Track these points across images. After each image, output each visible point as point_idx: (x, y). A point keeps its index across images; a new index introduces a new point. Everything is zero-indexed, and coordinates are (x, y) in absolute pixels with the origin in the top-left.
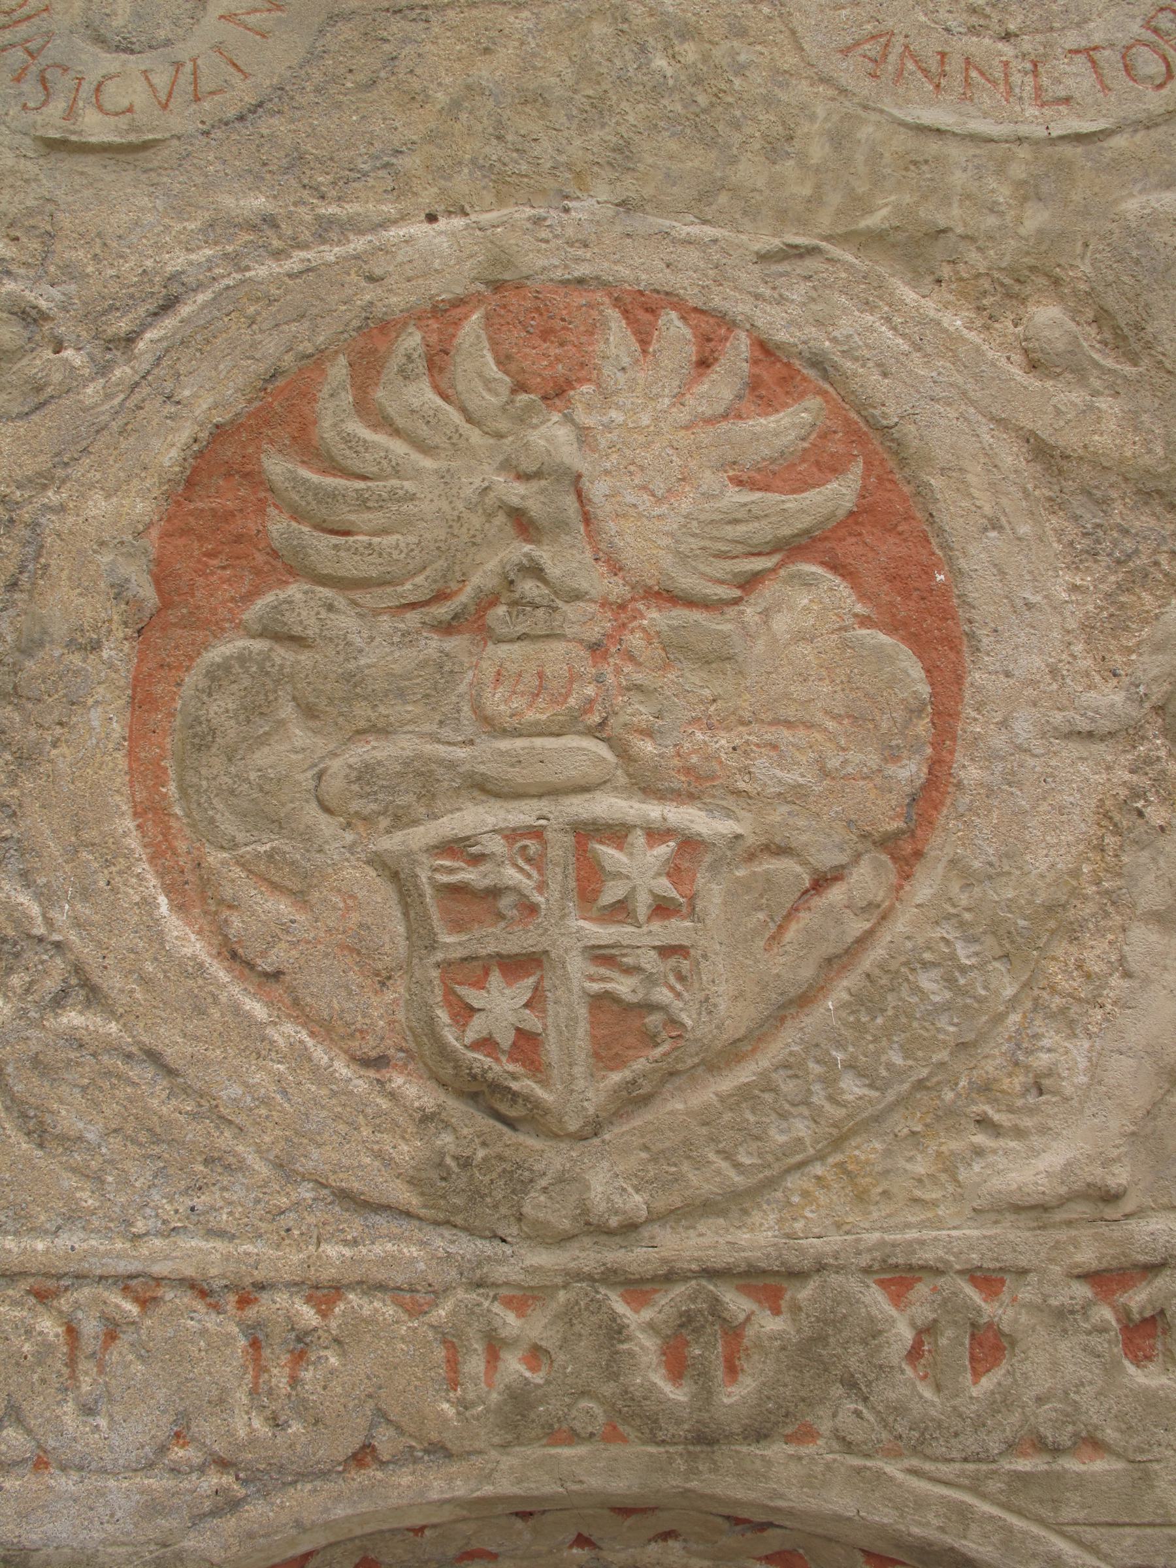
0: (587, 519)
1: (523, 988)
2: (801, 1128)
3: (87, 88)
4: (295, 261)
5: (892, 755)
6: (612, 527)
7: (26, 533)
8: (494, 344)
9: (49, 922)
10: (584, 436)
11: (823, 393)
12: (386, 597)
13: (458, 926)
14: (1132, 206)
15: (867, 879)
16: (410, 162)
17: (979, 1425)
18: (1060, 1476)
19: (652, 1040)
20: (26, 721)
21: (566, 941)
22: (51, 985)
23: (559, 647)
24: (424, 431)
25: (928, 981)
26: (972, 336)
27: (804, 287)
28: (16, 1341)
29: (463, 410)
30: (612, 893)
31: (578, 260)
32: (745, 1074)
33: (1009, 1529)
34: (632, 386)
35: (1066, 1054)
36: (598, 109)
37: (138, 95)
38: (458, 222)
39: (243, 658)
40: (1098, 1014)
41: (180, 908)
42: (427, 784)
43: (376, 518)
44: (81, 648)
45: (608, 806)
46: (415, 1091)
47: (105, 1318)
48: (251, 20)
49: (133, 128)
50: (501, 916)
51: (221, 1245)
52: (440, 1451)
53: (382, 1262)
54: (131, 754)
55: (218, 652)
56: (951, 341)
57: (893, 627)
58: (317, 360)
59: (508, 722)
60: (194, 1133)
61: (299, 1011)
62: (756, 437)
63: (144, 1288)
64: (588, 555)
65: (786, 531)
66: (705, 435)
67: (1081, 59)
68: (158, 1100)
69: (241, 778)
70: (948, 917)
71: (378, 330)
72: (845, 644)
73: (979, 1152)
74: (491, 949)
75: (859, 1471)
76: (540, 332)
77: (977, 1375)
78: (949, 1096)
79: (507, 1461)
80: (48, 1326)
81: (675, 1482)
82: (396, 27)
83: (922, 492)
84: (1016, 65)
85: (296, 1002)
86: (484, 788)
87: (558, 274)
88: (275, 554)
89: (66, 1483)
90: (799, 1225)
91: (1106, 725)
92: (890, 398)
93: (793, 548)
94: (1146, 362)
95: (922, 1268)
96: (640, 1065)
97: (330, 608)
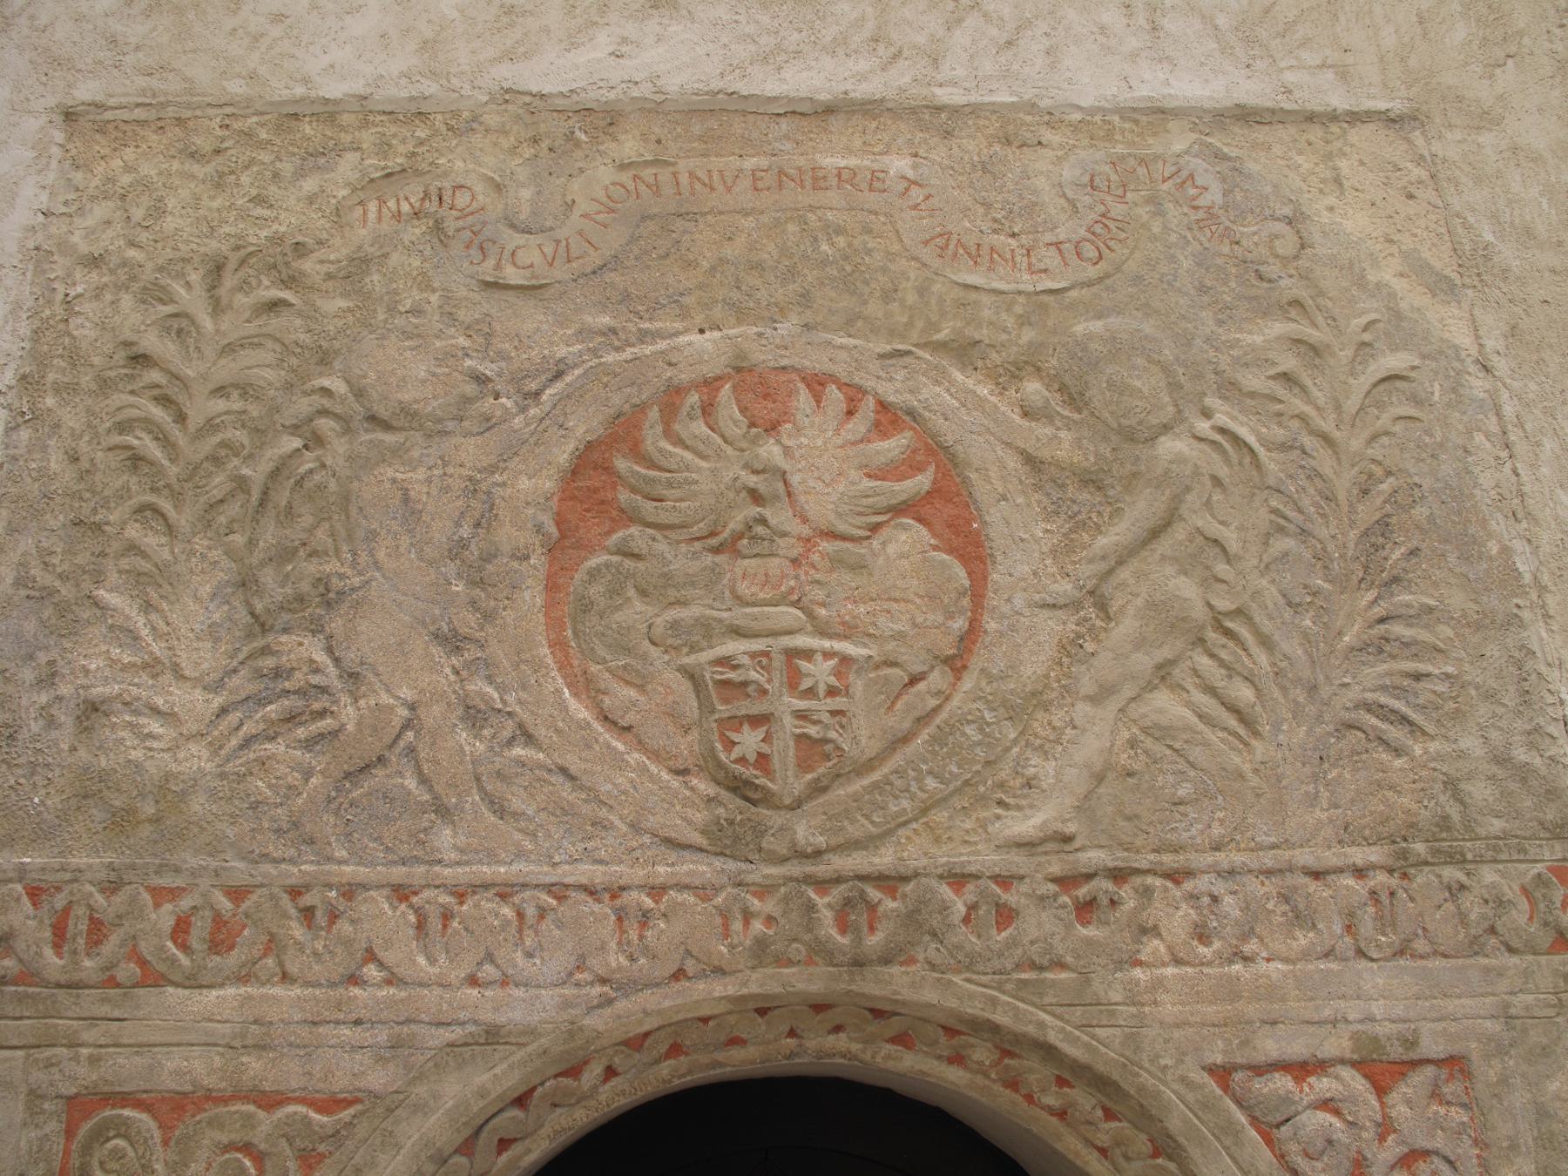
0: (789, 494)
1: (760, 733)
3: (507, 254)
4: (629, 353)
5: (950, 616)
6: (802, 498)
7: (485, 497)
8: (738, 401)
9: (504, 702)
10: (787, 451)
11: (913, 429)
12: (684, 534)
13: (726, 701)
14: (1079, 329)
15: (938, 678)
16: (688, 300)
17: (1001, 955)
18: (1043, 981)
19: (828, 757)
20: (488, 596)
21: (782, 708)
22: (507, 734)
23: (776, 561)
24: (701, 447)
26: (993, 399)
27: (903, 372)
28: (490, 919)
29: (722, 436)
30: (806, 684)
31: (782, 356)
32: (876, 776)
33: (1016, 1008)
34: (812, 425)
36: (792, 273)
37: (536, 258)
38: (717, 334)
39: (607, 565)
40: (1060, 748)
41: (575, 695)
42: (707, 630)
43: (677, 493)
44: (518, 558)
46: (704, 786)
47: (539, 907)
48: (599, 218)
49: (534, 277)
50: (748, 696)
51: (601, 868)
52: (719, 971)
53: (688, 874)
54: (546, 615)
55: (593, 562)
56: (981, 403)
57: (950, 552)
58: (642, 408)
59: (749, 599)
60: (586, 809)
61: (641, 745)
62: (878, 452)
63: (559, 891)
64: (790, 513)
65: (894, 502)
66: (851, 451)
67: (1052, 248)
68: (566, 792)
69: (608, 627)
70: (980, 698)
72: (925, 560)
73: (998, 817)
74: (743, 712)
75: (939, 980)
76: (762, 394)
77: (999, 931)
78: (982, 789)
79: (755, 976)
80: (507, 911)
81: (842, 986)
82: (679, 224)
83: (966, 481)
84: (1019, 251)
85: (640, 742)
86: (738, 632)
87: (771, 364)
88: (622, 511)
89: (519, 993)
90: (905, 854)
91: (1062, 601)
92: (949, 433)
93: (899, 510)
94: (1085, 412)
95: (970, 875)
96: (821, 770)
97: (654, 539)
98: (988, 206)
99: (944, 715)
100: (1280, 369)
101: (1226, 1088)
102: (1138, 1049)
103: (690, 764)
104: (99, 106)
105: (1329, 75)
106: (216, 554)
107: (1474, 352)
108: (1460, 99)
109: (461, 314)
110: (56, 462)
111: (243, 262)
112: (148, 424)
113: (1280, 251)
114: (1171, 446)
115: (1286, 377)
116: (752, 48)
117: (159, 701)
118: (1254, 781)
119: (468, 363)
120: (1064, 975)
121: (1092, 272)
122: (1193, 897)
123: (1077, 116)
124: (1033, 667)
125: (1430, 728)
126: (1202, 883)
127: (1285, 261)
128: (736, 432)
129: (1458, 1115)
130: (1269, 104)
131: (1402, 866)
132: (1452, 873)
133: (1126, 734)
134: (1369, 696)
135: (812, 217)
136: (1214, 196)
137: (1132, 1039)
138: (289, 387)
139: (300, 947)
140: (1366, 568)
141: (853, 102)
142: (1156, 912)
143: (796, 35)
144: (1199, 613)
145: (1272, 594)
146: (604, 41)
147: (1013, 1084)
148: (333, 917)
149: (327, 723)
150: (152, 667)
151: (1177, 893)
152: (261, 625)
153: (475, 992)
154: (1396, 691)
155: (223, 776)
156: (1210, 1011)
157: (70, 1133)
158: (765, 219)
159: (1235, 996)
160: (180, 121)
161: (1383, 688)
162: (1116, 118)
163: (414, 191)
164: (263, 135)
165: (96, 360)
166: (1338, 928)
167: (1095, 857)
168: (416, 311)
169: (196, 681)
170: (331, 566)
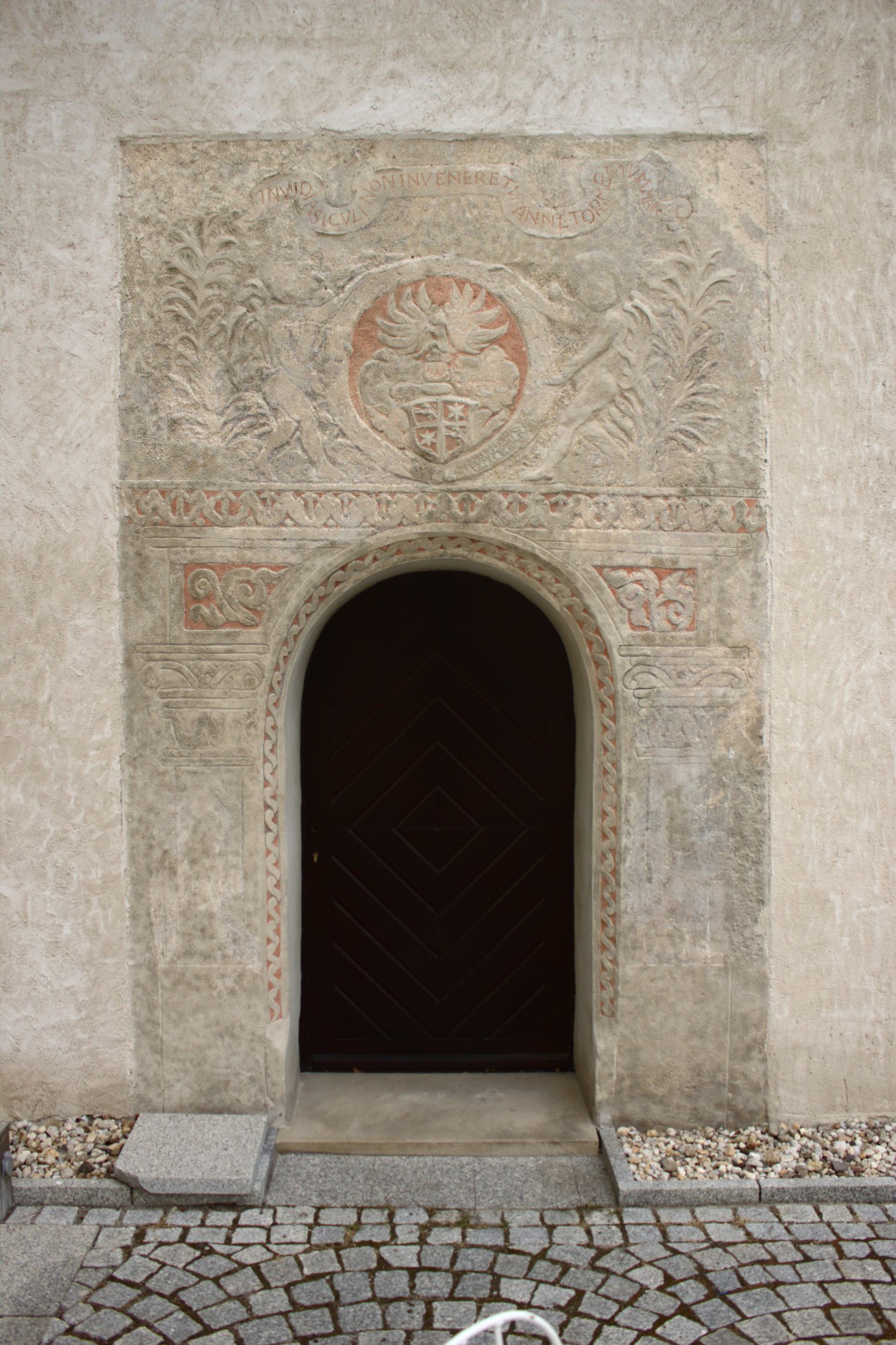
1: (433, 434)
2: (487, 463)
5: (510, 388)
10: (447, 315)
14: (579, 257)
15: (503, 414)
16: (408, 242)
22: (335, 433)
25: (515, 435)
30: (451, 415)
32: (476, 452)
35: (542, 451)
36: (453, 229)
42: (413, 392)
45: (451, 397)
46: (411, 454)
49: (340, 230)
52: (415, 523)
55: (368, 363)
56: (531, 294)
57: (513, 360)
58: (387, 294)
60: (366, 462)
63: (356, 493)
68: (359, 456)
71: (401, 286)
76: (437, 286)
80: (337, 500)
82: (403, 203)
83: (522, 329)
86: (425, 393)
89: (342, 530)
93: (492, 342)
98: (544, 192)
99: (504, 429)
100: (669, 277)
101: (601, 574)
102: (568, 558)
103: (406, 445)
104: (135, 138)
105: (724, 112)
106: (215, 358)
107: (764, 268)
108: (790, 125)
109: (309, 248)
110: (144, 318)
111: (211, 221)
112: (181, 301)
113: (680, 215)
114: (613, 314)
115: (671, 281)
116: (439, 103)
117: (200, 419)
118: (627, 459)
119: (313, 272)
120: (543, 530)
121: (588, 227)
122: (597, 503)
123: (592, 140)
124: (543, 409)
125: (706, 441)
126: (600, 499)
127: (682, 219)
128: (426, 306)
129: (689, 589)
130: (690, 131)
131: (684, 495)
132: (704, 500)
133: (577, 439)
134: (682, 427)
135: (463, 199)
136: (653, 185)
137: (567, 555)
138: (238, 283)
139: (262, 512)
140: (691, 371)
141: (485, 135)
142: (581, 508)
143: (460, 95)
144: (614, 389)
145: (647, 381)
146: (368, 99)
147: (523, 569)
148: (274, 501)
149: (266, 428)
150: (195, 405)
151: (590, 501)
152: (236, 388)
153: (326, 529)
154: (695, 425)
155: (228, 449)
156: (598, 546)
157: (186, 576)
158: (442, 200)
159: (608, 541)
160: (173, 145)
161: (689, 424)
162: (612, 140)
163: (284, 184)
164: (213, 153)
165: (154, 270)
166: (653, 518)
167: (560, 486)
168: (289, 247)
169: (213, 411)
170: (263, 364)
